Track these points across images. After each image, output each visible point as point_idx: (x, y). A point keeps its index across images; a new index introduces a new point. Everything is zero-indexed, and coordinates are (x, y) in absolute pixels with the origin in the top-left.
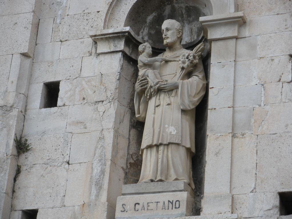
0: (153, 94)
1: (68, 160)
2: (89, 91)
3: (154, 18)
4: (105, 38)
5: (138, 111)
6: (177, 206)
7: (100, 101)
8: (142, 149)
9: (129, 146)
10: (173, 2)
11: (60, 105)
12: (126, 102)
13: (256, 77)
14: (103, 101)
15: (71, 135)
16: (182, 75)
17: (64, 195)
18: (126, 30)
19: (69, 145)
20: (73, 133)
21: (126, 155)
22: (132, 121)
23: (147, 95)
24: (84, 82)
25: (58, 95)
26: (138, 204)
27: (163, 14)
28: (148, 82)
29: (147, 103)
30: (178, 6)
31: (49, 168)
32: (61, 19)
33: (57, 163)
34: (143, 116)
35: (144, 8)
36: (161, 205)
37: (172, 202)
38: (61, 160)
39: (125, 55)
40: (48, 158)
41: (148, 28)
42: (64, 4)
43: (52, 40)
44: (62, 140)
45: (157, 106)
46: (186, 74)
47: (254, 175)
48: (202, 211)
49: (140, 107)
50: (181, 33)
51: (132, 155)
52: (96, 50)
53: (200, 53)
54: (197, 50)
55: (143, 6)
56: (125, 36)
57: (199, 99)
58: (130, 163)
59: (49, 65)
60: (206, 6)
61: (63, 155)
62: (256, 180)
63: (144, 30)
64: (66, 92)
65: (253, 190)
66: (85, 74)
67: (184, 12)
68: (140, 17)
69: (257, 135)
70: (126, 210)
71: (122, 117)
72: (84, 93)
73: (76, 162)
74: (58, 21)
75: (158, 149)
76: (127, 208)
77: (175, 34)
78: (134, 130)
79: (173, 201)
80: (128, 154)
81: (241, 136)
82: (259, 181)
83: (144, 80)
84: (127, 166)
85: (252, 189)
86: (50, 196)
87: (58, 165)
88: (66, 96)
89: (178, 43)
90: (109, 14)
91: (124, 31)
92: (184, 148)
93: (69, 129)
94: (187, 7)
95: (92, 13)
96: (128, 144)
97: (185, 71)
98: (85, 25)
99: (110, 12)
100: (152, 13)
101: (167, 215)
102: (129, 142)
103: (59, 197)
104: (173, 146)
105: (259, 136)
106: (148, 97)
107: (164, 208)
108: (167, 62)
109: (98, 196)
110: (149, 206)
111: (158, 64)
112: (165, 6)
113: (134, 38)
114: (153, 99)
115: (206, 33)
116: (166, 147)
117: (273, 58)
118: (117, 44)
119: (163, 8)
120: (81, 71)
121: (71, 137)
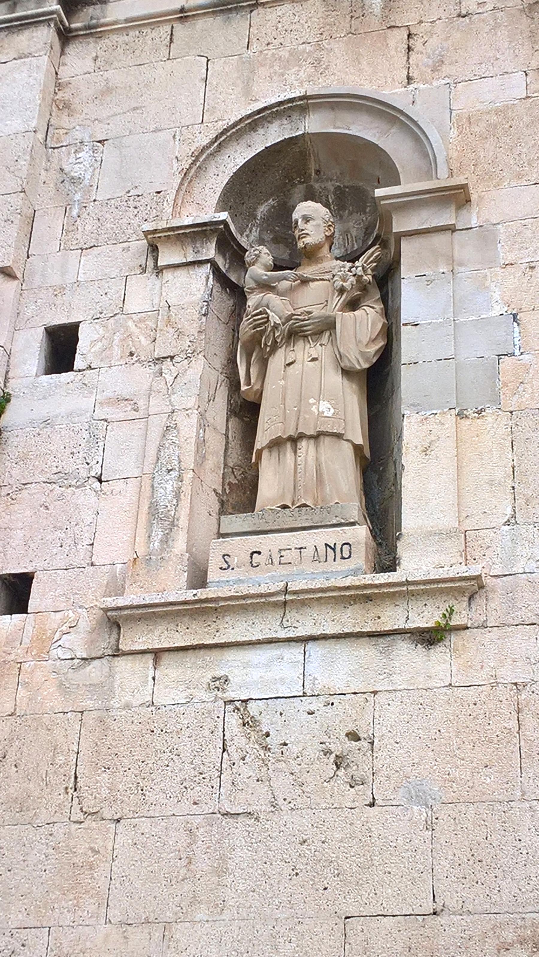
0: (279, 341)
1: (99, 473)
2: (142, 338)
3: (269, 210)
4: (175, 235)
5: (245, 379)
6: (346, 554)
7: (167, 358)
8: (258, 449)
9: (226, 450)
10: (311, 178)
11: (80, 368)
12: (219, 362)
13: (499, 302)
14: (172, 358)
15: (106, 423)
16: (339, 304)
17: (91, 543)
18: (219, 219)
19: (101, 444)
20: (109, 420)
21: (222, 466)
22: (232, 402)
23: (265, 344)
24: (130, 323)
25: (76, 349)
26: (259, 553)
27: (289, 204)
28: (268, 318)
29: (264, 364)
30: (321, 187)
31: (58, 490)
32: (80, 209)
33: (76, 481)
34: (257, 387)
35: (252, 186)
36: (309, 552)
37: (333, 547)
38: (84, 474)
39: (216, 269)
40: (55, 470)
41: (259, 229)
42: (86, 182)
43: (62, 247)
44: (86, 435)
45: (289, 365)
46: (347, 304)
47: (509, 490)
48: (399, 564)
49: (251, 370)
50: (332, 229)
51: (232, 469)
52: (156, 260)
53: (375, 264)
54: (369, 258)
55: (249, 183)
56: (216, 232)
57: (377, 351)
58: (230, 484)
59: (55, 293)
60: (379, 182)
61: (88, 464)
62: (515, 499)
63: (251, 231)
64: (93, 343)
65: (509, 521)
66: (130, 307)
67: (331, 201)
68: (243, 204)
69: (511, 412)
70: (232, 567)
71: (212, 392)
72: (130, 343)
73: (117, 477)
74: (75, 212)
75: (296, 446)
76: (234, 561)
77: (322, 229)
78: (237, 419)
79: (335, 544)
80: (226, 465)
81: (476, 415)
82: (520, 501)
83: (260, 313)
84: (224, 490)
85: (507, 517)
86: (60, 545)
87: (78, 483)
88: (92, 350)
89: (327, 247)
90: (182, 193)
91: (215, 220)
92: (350, 445)
93: (100, 413)
94: (338, 188)
95: (144, 195)
96: (226, 445)
97: (346, 297)
98: (132, 217)
99: (184, 188)
100: (267, 200)
101: (323, 573)
102: (227, 443)
103: (80, 546)
104: (327, 440)
105: (514, 413)
106: (268, 349)
107: (316, 559)
108: (305, 281)
109: (165, 541)
110: (281, 556)
111: (285, 285)
112: (294, 185)
113: (235, 239)
114: (280, 353)
115: (387, 221)
116: (312, 442)
117: (532, 265)
118: (200, 249)
119: (288, 191)
120: (124, 303)
121: (105, 428)
